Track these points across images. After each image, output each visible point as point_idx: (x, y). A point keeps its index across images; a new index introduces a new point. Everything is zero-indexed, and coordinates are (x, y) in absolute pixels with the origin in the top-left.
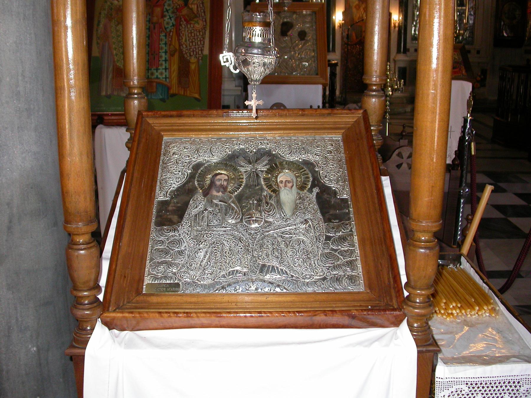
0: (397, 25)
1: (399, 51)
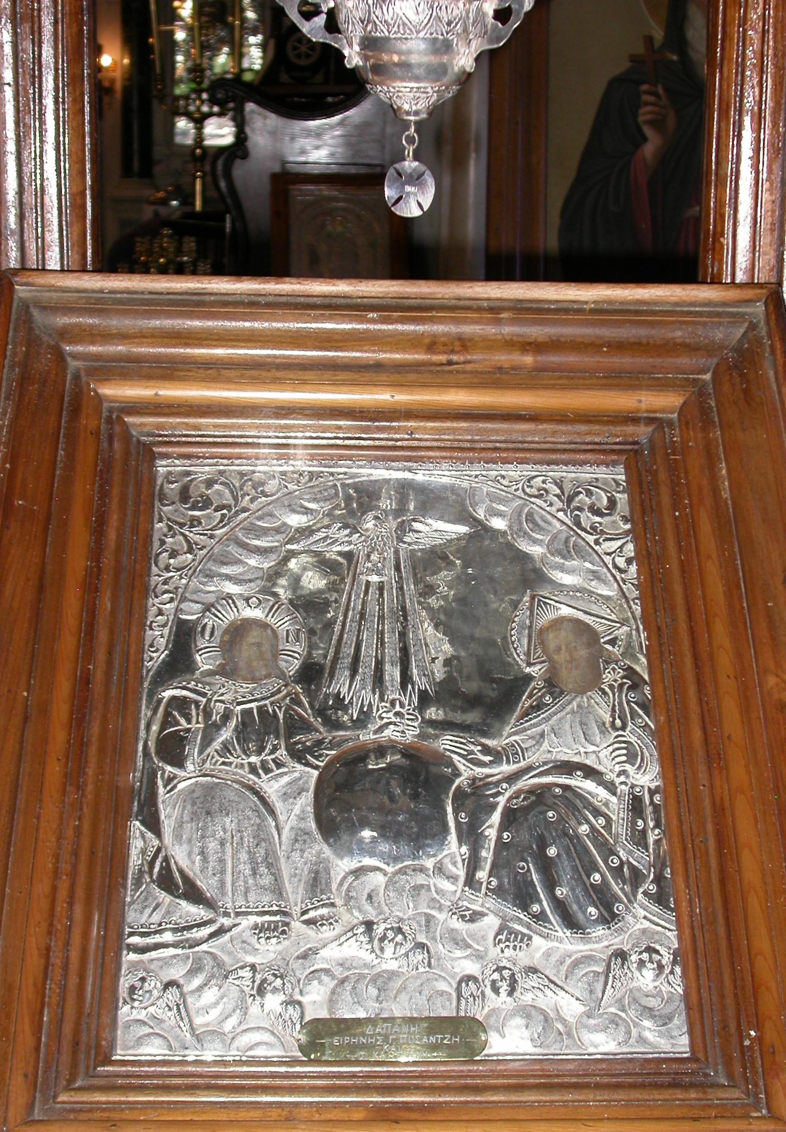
0: (118, 86)
1: (127, 171)
